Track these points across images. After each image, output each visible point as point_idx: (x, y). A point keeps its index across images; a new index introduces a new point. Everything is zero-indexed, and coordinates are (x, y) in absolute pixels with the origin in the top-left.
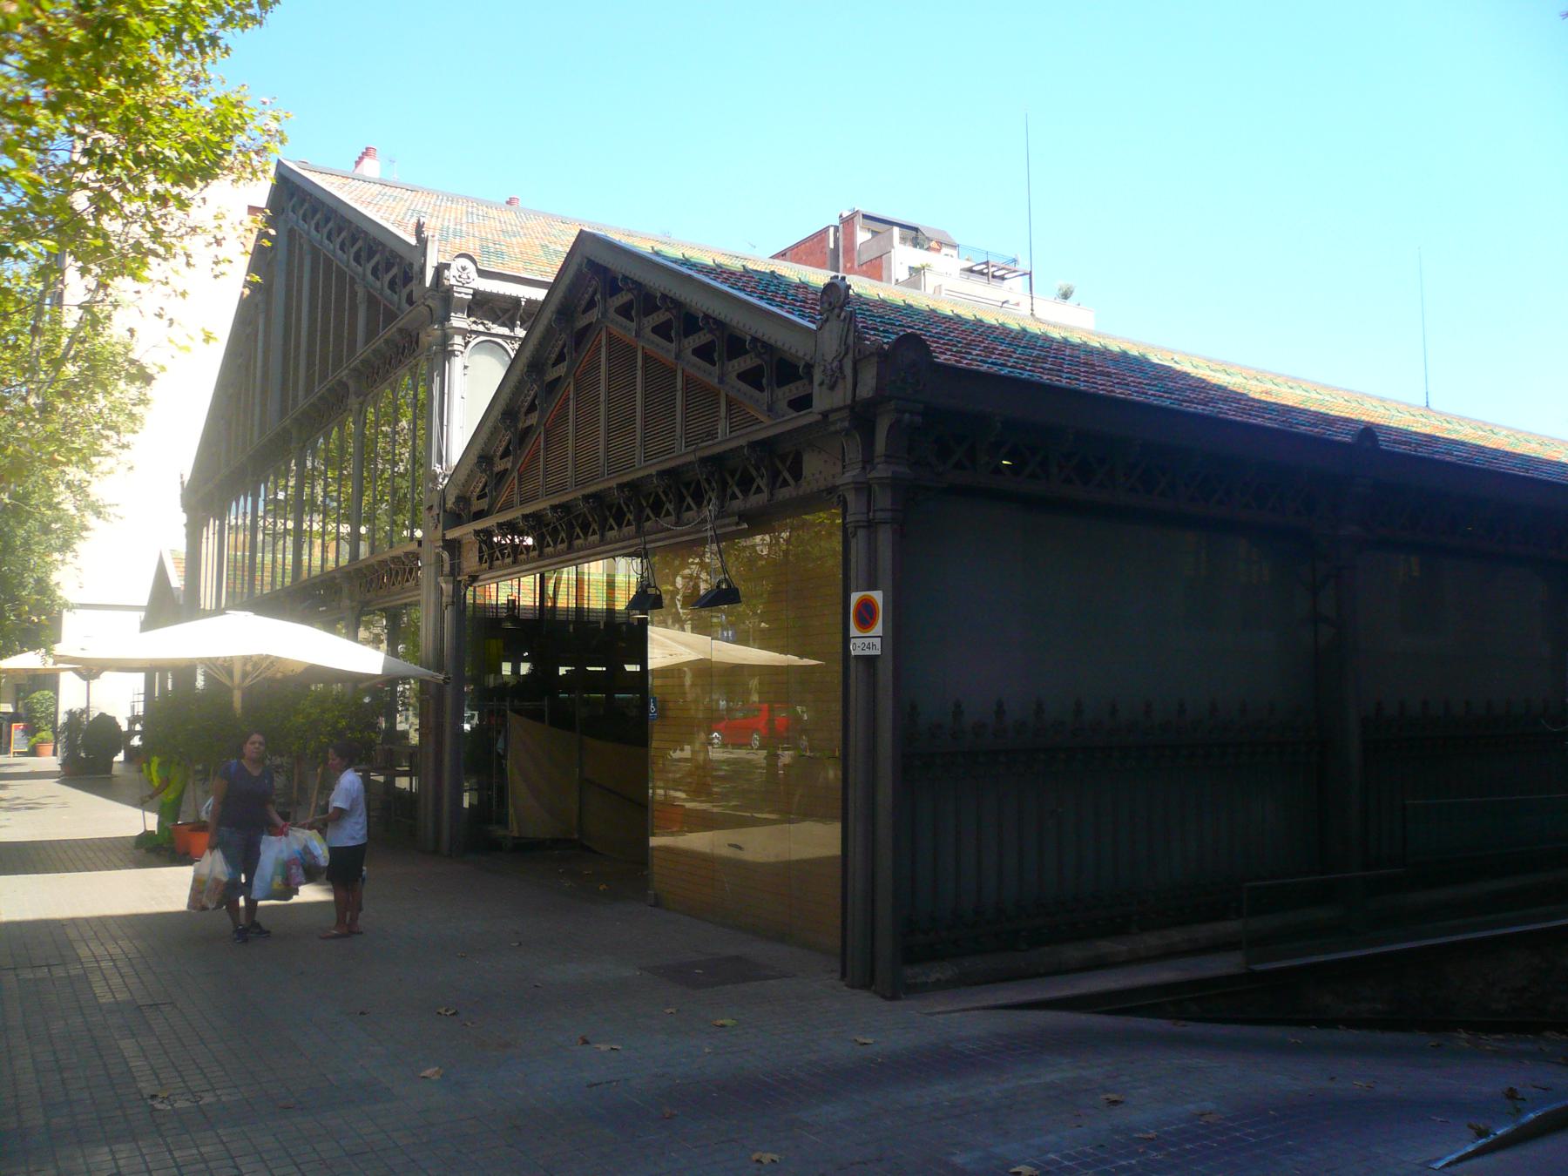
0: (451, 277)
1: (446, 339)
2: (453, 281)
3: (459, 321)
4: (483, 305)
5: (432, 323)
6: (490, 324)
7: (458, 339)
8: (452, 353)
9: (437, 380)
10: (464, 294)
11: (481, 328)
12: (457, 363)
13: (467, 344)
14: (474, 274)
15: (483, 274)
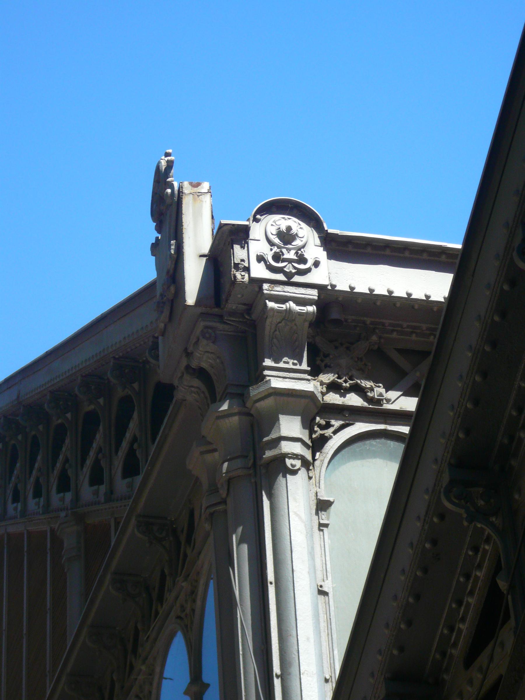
0: (254, 258)
1: (258, 429)
2: (259, 271)
3: (286, 376)
4: (346, 334)
5: (215, 398)
6: (379, 390)
7: (290, 426)
8: (279, 467)
9: (241, 554)
10: (295, 301)
11: (353, 400)
12: (296, 494)
13: (318, 444)
14: (315, 251)
15: (342, 248)
